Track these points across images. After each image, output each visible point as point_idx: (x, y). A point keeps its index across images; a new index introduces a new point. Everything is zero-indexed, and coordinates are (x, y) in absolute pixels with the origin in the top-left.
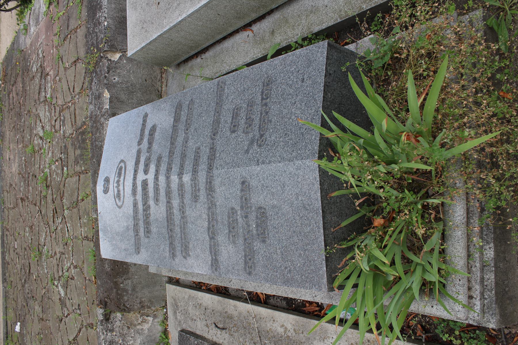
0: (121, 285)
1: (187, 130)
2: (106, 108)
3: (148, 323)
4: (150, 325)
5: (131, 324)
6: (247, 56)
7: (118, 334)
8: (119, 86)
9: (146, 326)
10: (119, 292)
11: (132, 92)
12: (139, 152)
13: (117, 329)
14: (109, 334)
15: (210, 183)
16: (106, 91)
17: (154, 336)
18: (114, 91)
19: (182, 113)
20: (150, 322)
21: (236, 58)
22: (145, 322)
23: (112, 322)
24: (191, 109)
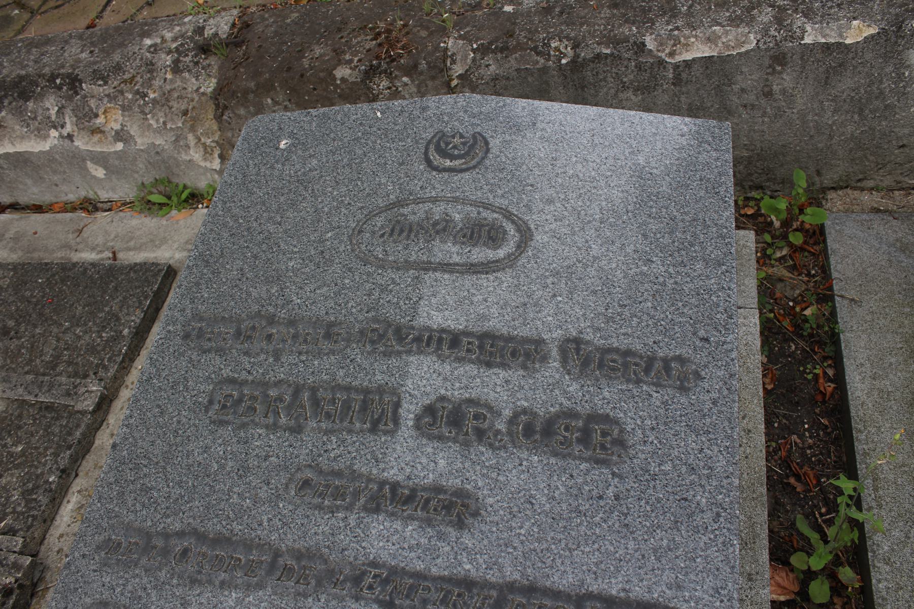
0: (269, 101)
2: (804, 31)
3: (205, 160)
4: (203, 164)
5: (194, 119)
7: (168, 87)
8: (889, 69)
9: (196, 155)
10: (251, 96)
11: (861, 110)
12: (521, 352)
13: (179, 83)
14: (169, 59)
16: (873, 30)
17: (181, 173)
18: (869, 56)
20: (208, 165)
22: (206, 152)
23: (197, 63)
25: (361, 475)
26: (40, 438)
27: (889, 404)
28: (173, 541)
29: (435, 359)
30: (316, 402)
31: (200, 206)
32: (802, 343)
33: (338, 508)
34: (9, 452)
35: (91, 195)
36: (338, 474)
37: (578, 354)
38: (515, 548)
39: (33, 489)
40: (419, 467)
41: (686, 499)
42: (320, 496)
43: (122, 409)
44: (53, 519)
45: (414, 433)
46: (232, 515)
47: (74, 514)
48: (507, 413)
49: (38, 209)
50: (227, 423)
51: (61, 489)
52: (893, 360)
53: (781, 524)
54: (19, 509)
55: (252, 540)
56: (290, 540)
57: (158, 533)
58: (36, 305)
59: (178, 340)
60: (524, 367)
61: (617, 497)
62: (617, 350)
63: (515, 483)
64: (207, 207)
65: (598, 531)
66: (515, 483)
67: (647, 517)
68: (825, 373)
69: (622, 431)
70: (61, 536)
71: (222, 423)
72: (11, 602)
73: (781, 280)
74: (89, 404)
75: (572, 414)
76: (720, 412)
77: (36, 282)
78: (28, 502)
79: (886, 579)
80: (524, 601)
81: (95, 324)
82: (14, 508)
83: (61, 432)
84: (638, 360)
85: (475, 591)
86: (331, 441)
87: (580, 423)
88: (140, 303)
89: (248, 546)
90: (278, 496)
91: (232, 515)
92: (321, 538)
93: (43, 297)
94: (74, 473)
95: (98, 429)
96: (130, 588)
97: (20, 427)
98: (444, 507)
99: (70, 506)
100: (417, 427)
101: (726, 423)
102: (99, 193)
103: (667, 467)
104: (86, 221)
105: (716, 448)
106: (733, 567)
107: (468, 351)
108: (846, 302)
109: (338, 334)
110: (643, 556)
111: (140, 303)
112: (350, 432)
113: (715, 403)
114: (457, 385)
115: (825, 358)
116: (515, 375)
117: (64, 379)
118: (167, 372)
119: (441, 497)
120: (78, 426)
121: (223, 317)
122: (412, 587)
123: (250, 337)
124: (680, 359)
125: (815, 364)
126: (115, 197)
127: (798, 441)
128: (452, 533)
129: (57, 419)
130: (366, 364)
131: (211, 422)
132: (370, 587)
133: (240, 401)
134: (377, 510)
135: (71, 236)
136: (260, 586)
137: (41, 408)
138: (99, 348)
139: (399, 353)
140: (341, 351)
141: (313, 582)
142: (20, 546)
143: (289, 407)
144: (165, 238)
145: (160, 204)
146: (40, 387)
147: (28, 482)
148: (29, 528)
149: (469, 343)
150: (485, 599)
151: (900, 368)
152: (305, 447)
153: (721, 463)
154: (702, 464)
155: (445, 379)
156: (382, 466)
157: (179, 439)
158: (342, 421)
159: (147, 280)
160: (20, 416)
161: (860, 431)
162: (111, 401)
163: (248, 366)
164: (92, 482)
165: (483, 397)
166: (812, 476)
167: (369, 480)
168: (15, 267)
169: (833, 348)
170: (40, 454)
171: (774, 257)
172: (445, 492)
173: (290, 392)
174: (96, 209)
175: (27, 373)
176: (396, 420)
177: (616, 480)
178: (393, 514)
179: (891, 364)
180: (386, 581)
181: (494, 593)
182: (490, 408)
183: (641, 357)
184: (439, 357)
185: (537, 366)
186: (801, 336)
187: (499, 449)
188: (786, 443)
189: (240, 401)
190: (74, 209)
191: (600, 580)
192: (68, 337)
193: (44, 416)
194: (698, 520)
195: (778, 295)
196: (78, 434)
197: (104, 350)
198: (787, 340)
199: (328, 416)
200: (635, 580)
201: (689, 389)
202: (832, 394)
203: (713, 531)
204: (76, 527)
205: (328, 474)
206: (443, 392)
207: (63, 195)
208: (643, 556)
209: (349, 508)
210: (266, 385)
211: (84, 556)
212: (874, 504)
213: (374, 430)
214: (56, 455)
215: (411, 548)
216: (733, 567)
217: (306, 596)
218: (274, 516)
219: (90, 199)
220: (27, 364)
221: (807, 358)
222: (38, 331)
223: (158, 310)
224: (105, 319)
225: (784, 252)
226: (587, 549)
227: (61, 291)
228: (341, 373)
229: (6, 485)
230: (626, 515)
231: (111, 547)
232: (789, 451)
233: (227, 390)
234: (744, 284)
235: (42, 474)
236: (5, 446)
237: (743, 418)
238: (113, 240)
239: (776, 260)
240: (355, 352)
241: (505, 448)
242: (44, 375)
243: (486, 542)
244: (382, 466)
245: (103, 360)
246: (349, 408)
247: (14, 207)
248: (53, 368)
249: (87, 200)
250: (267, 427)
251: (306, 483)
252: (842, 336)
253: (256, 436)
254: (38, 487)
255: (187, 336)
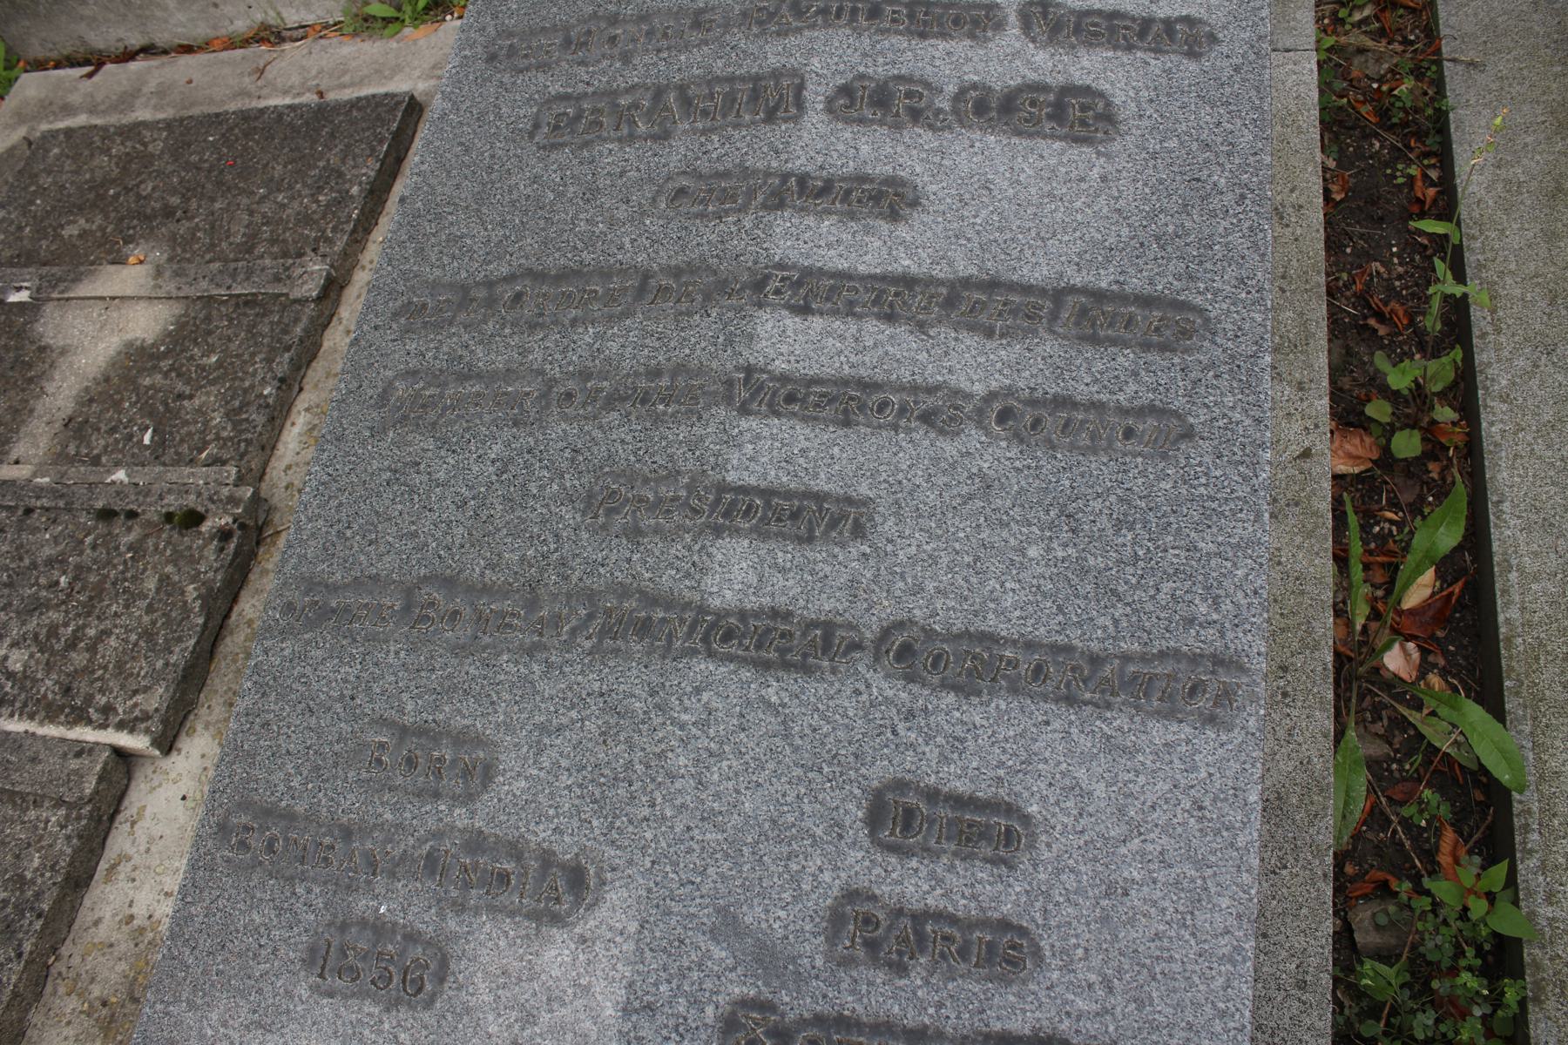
1: (1004, 416)
6: (1527, 529)
15: (644, 628)
19: (1126, 359)
21: (1539, 448)
24: (1129, 433)
25: (755, 172)
26: (242, 343)
27: (1520, 198)
28: (499, 290)
29: (848, 32)
30: (686, 102)
31: (448, 17)
32: (1392, 139)
33: (727, 212)
34: (198, 366)
35: (272, 19)
36: (726, 175)
37: (1045, 18)
38: (969, 240)
39: (241, 408)
40: (835, 155)
41: (1198, 180)
42: (701, 202)
43: (359, 297)
44: (274, 448)
45: (824, 117)
46: (580, 245)
47: (304, 439)
48: (951, 89)
49: (187, 49)
50: (563, 145)
51: (282, 406)
52: (1529, 139)
53: (1354, 380)
54: (225, 434)
55: (610, 267)
56: (666, 256)
57: (477, 284)
58: (209, 172)
59: (480, 65)
60: (972, 36)
61: (1104, 179)
62: (1099, 12)
63: (965, 168)
64: (460, 17)
65: (1079, 217)
66: (965, 168)
67: (1145, 200)
68: (1425, 176)
69: (1109, 104)
70: (289, 467)
71: (554, 147)
72: (232, 546)
73: (1361, 51)
74: (311, 289)
75: (1042, 88)
76: (1244, 80)
77: (205, 140)
78: (235, 425)
79: (1502, 421)
80: (984, 298)
81: (305, 185)
82: (217, 434)
83: (272, 330)
84: (1128, 23)
85: (918, 289)
86: (712, 142)
87: (1052, 97)
88: (373, 149)
89: (605, 274)
90: (643, 214)
91: (580, 245)
92: (706, 248)
93: (219, 160)
94: (297, 388)
95: (326, 326)
96: (445, 349)
97: (210, 333)
98: (870, 198)
99: (296, 430)
100: (830, 108)
101: (1253, 93)
102: (285, 15)
103: (1173, 143)
104: (267, 57)
105: (1239, 122)
106: (1264, 255)
107: (894, 21)
108: (1460, 68)
109: (711, 21)
110: (1142, 244)
111: (373, 149)
112: (737, 126)
113: (1237, 69)
114: (881, 60)
115: (1427, 155)
116: (960, 46)
117: (268, 262)
118: (468, 103)
119: (866, 187)
120: (297, 320)
121: (543, 28)
122: (832, 289)
123: (585, 44)
124: (1187, 20)
125: (1409, 162)
126: (310, 19)
127: (1382, 270)
128: (884, 226)
129: (264, 315)
130: (753, 48)
131: (539, 148)
132: (777, 292)
133: (578, 117)
134: (781, 205)
135: (247, 80)
136: (627, 314)
137: (237, 305)
138: (316, 217)
139: (799, 30)
140: (717, 39)
141: (699, 298)
142: (233, 477)
143: (650, 113)
144: (398, 65)
145: (384, 19)
146: (234, 275)
147: (233, 398)
148: (242, 456)
149: (894, 12)
150: (932, 297)
151: (1539, 149)
152: (677, 153)
153: (1246, 138)
154: (1219, 140)
155: (865, 55)
156: (784, 157)
157: (493, 176)
158: (724, 116)
159: (379, 117)
160: (208, 319)
161: (1474, 238)
162: (342, 288)
163: (586, 77)
164: (324, 395)
165: (917, 74)
166: (1401, 313)
167: (767, 174)
168: (168, 125)
169: (1438, 138)
170: (245, 362)
171: (1350, 20)
172: (872, 181)
173: (649, 95)
174: (282, 40)
175: (210, 262)
176: (800, 104)
177: (1102, 160)
178: (802, 209)
179: (1526, 145)
180: (799, 284)
181: (944, 291)
182: (927, 85)
183: (1133, 19)
184: (854, 29)
185: (990, 34)
186: (1391, 128)
187: (942, 129)
188: (1363, 273)
189: (578, 117)
190: (246, 42)
191: (1084, 272)
192: (266, 208)
193: (245, 314)
194: (1215, 202)
195: (1355, 73)
196: (298, 330)
197: (324, 217)
198: (1366, 136)
199: (705, 113)
200: (1132, 271)
201: (1201, 55)
202: (1435, 201)
203: (1235, 215)
204: (309, 454)
205: (711, 177)
206: (862, 69)
207: (227, 23)
208: (1142, 244)
209: (743, 209)
210: (615, 93)
211: (376, 328)
212: (1489, 329)
213: (770, 118)
214: (269, 361)
215: (829, 246)
216: (1264, 255)
217: (689, 314)
218: (640, 235)
219: (270, 26)
220: (208, 251)
221: (1397, 159)
222: (217, 205)
223: (400, 161)
224: (321, 177)
225: (1367, 12)
226: (1067, 238)
227: (245, 148)
228: (720, 63)
229: (201, 406)
230: (1117, 199)
231: (411, 311)
232: (1368, 285)
233: (559, 108)
234: (1294, 19)
235: (252, 386)
236: (192, 358)
237: (1292, 191)
238: (316, 77)
239: (1353, 25)
240: (737, 37)
241: (949, 128)
242: (236, 260)
243: (929, 234)
244: (784, 157)
245: (324, 232)
246: (734, 100)
247: (148, 50)
248: (250, 251)
249: (265, 27)
250: (620, 140)
251: (681, 192)
252: (1451, 115)
253: (606, 152)
254: (248, 404)
255: (492, 58)
